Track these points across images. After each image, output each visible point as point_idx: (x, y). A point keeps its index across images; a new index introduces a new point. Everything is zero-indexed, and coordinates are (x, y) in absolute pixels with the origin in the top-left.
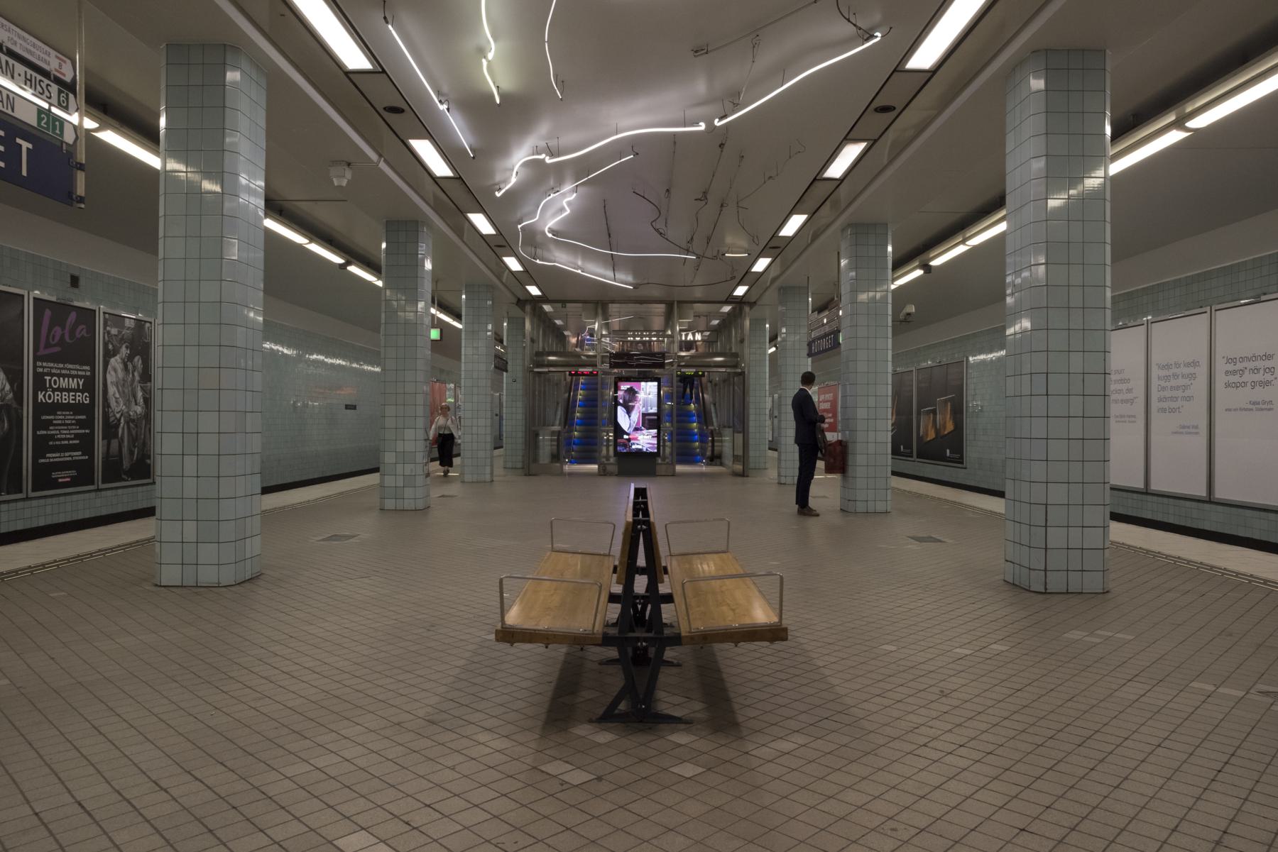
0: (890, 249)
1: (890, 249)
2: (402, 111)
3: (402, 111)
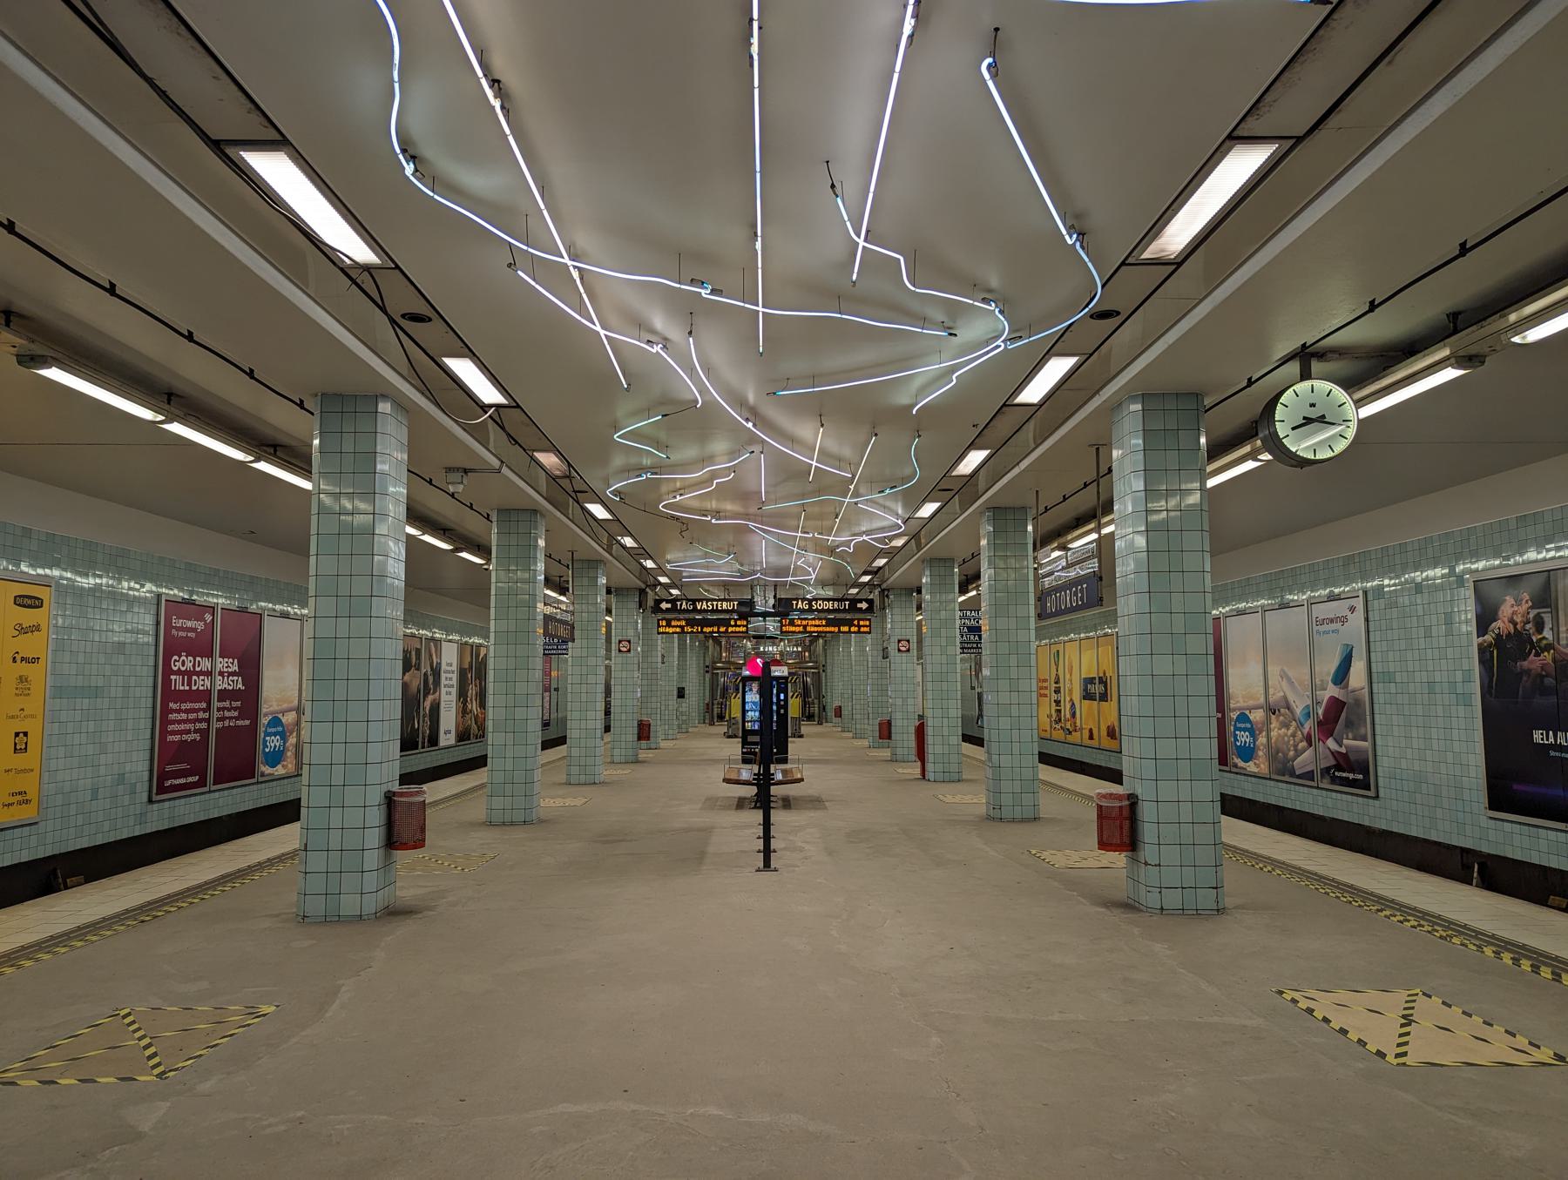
0: (1203, 440)
1: (1203, 440)
2: (403, 316)
3: (403, 316)
